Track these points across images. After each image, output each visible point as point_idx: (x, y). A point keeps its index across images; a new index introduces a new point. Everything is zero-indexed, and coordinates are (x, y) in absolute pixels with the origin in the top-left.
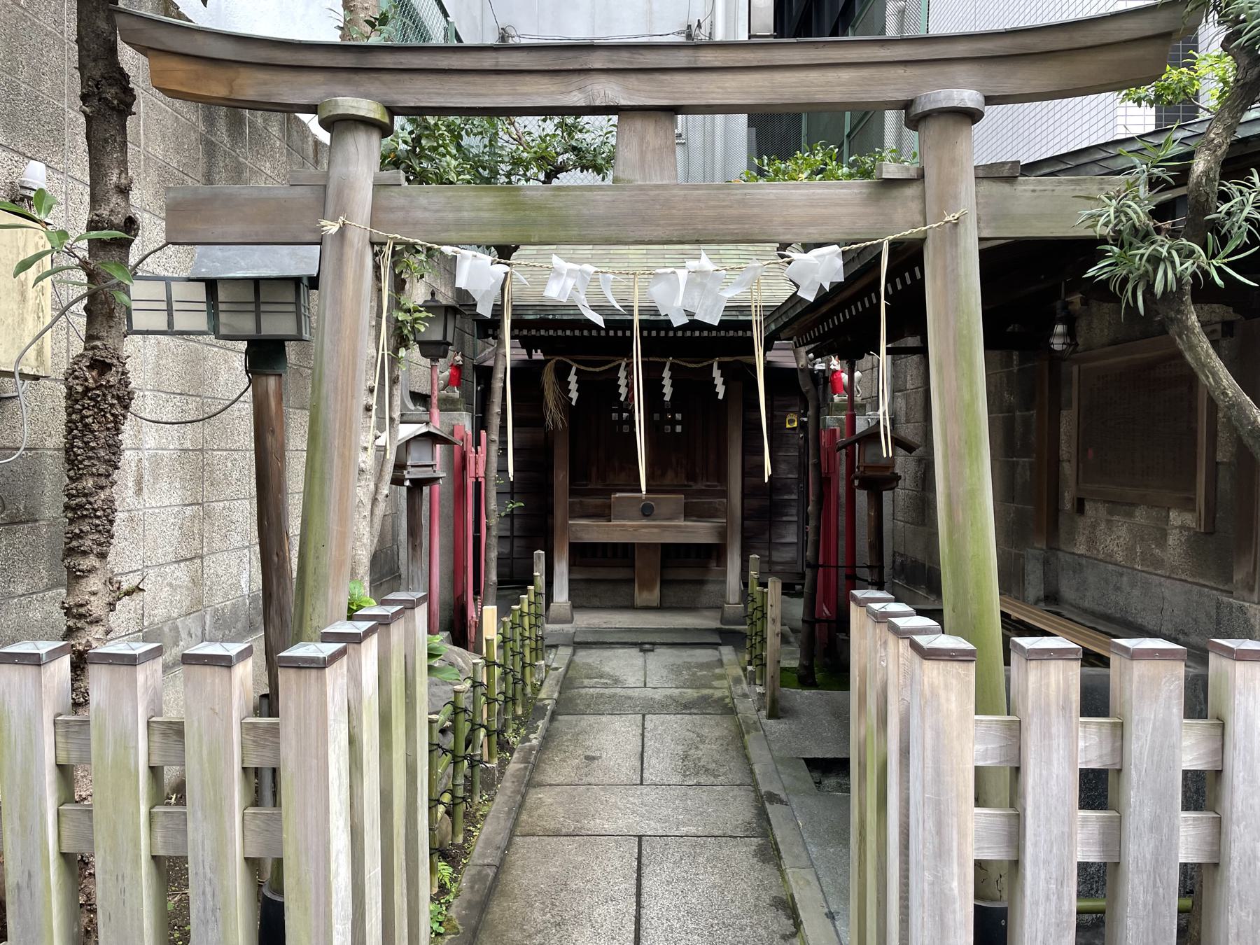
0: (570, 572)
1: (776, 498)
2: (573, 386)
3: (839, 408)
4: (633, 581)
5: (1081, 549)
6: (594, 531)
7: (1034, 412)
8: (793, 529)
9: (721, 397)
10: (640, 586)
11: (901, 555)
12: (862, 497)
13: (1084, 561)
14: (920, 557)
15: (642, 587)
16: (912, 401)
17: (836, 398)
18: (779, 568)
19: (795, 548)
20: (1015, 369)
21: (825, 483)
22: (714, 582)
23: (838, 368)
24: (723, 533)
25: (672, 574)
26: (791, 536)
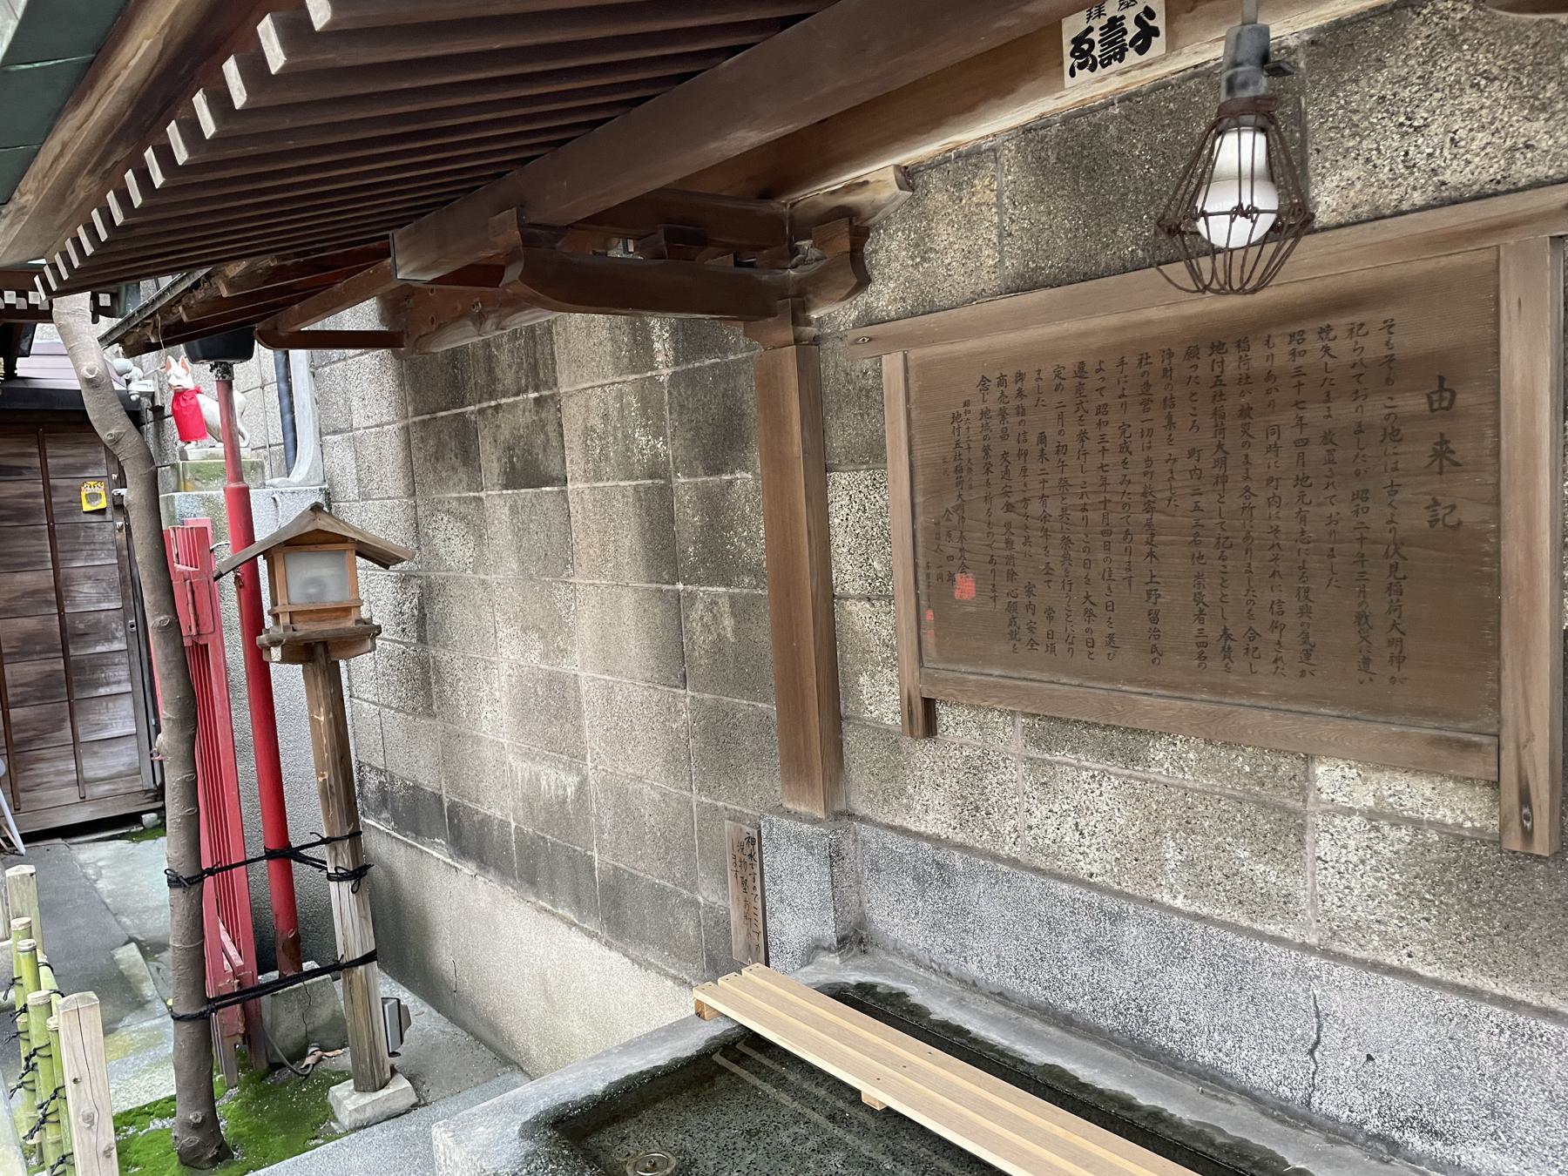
3: (203, 474)
5: (937, 821)
7: (744, 479)
8: (125, 707)
11: (380, 772)
12: (288, 680)
13: (957, 860)
14: (428, 780)
16: (370, 454)
17: (194, 451)
18: (103, 789)
19: (133, 742)
20: (664, 374)
21: (194, 659)
23: (188, 384)
26: (121, 720)
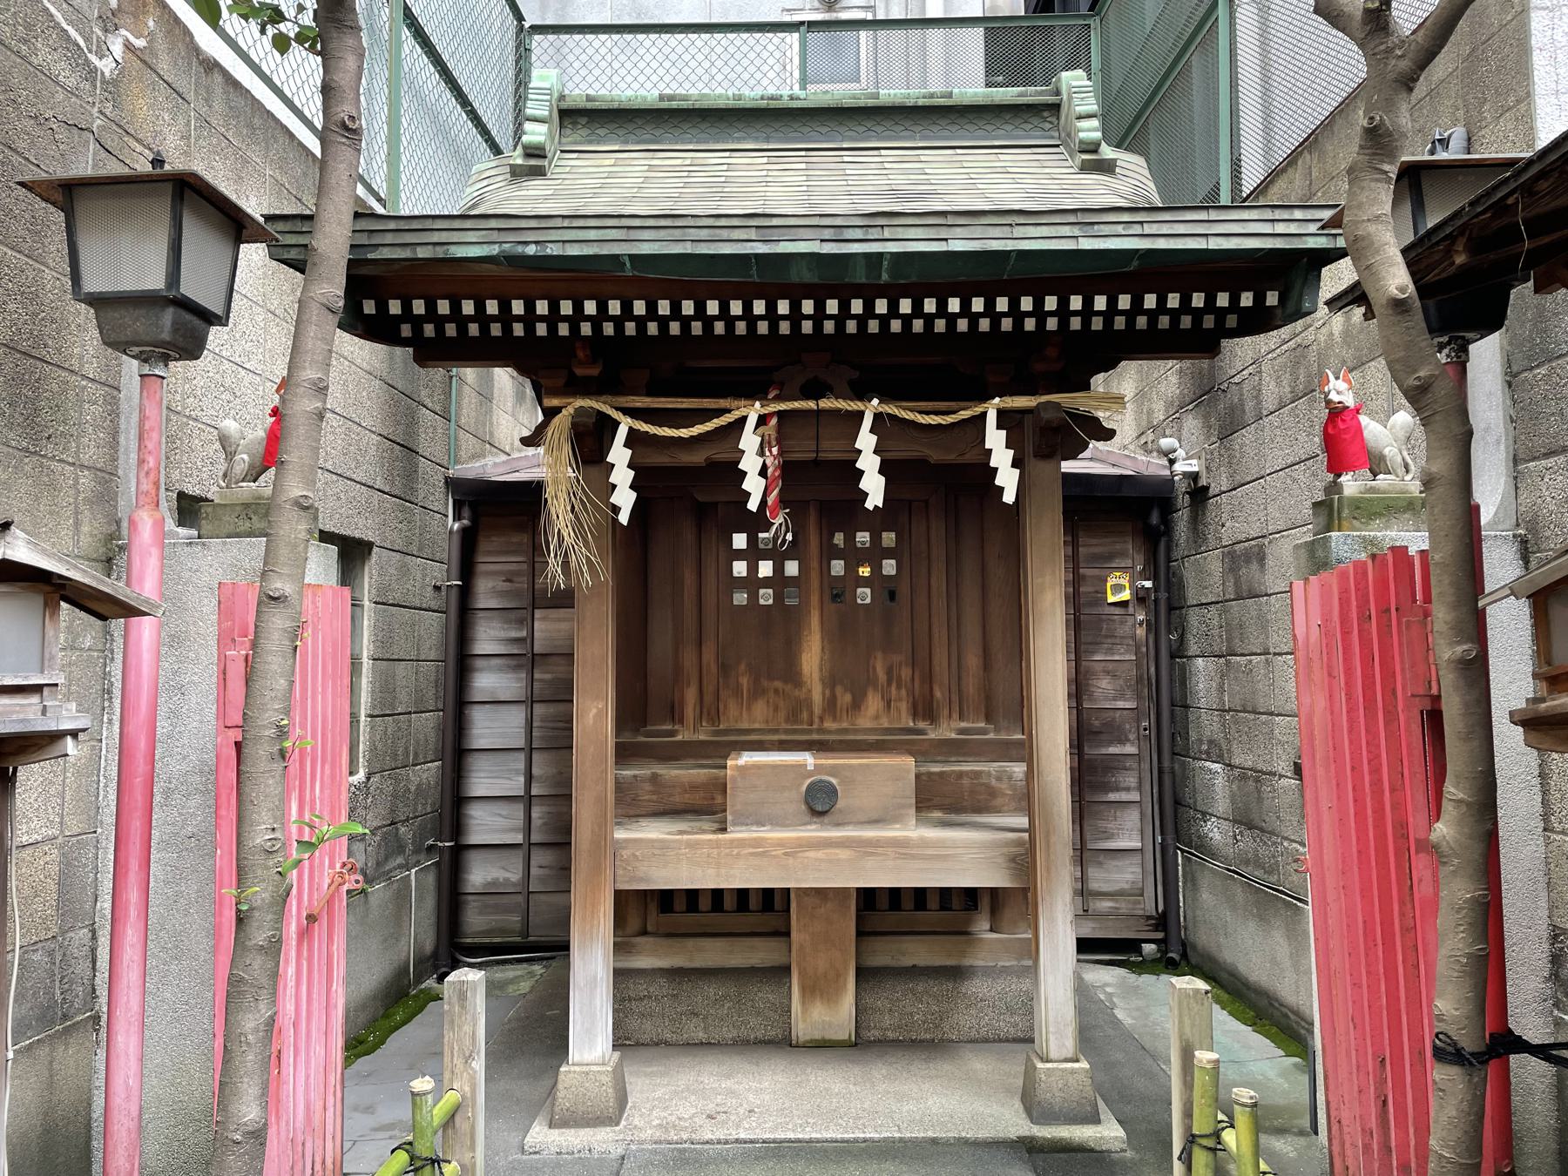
0: (620, 948)
1: (1091, 751)
2: (622, 476)
4: (785, 970)
6: (675, 855)
8: (1132, 818)
9: (1009, 497)
10: (804, 990)
15: (810, 991)
18: (1105, 905)
22: (992, 972)
24: (1024, 860)
25: (885, 954)
